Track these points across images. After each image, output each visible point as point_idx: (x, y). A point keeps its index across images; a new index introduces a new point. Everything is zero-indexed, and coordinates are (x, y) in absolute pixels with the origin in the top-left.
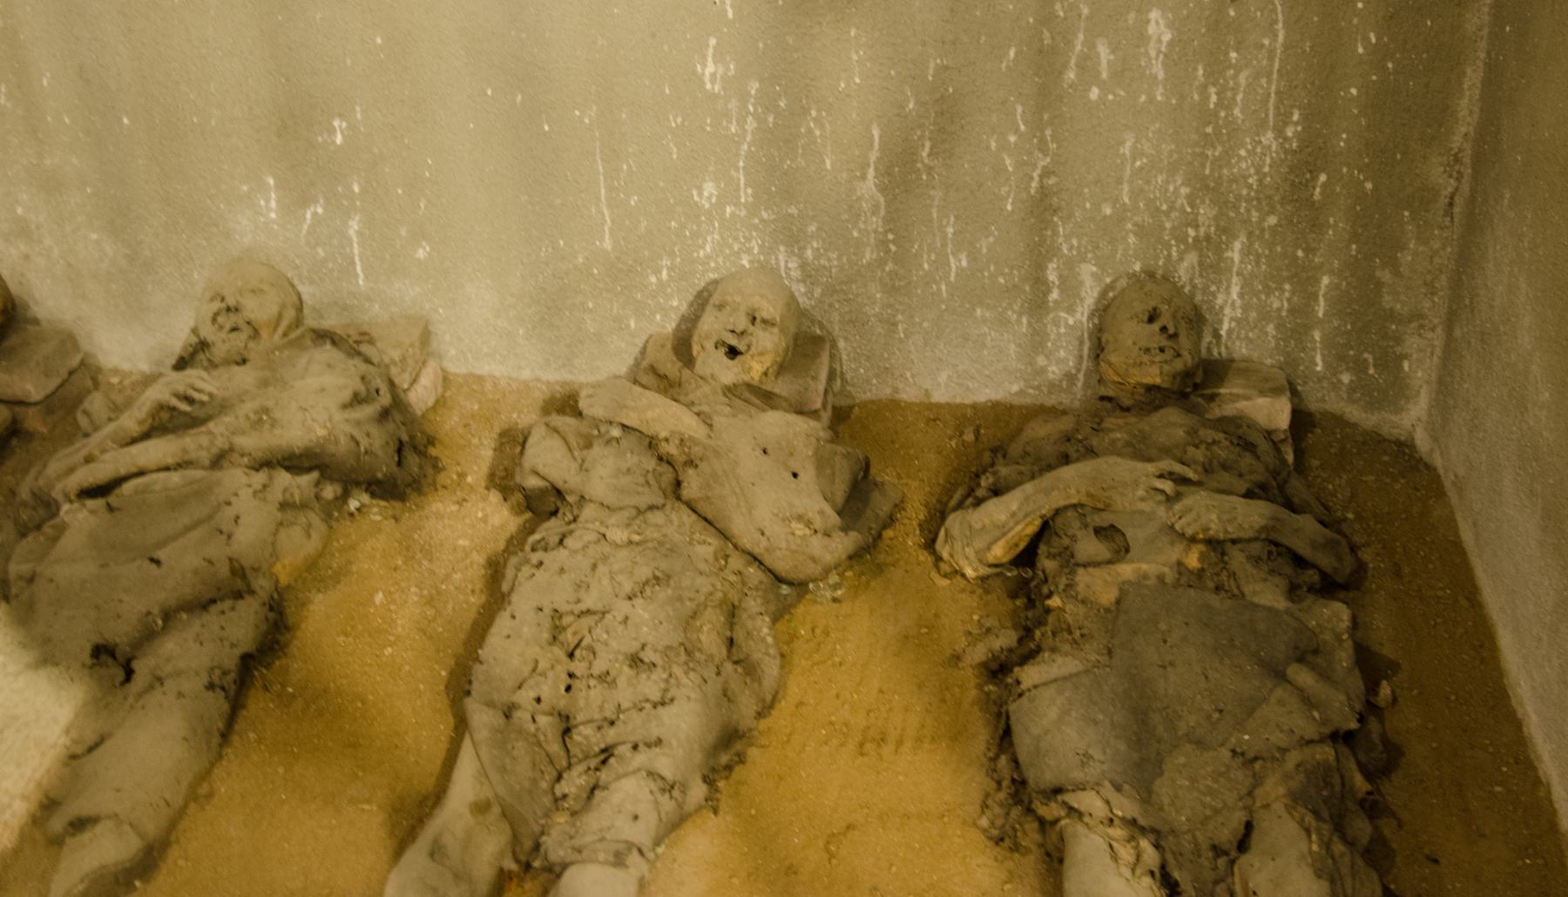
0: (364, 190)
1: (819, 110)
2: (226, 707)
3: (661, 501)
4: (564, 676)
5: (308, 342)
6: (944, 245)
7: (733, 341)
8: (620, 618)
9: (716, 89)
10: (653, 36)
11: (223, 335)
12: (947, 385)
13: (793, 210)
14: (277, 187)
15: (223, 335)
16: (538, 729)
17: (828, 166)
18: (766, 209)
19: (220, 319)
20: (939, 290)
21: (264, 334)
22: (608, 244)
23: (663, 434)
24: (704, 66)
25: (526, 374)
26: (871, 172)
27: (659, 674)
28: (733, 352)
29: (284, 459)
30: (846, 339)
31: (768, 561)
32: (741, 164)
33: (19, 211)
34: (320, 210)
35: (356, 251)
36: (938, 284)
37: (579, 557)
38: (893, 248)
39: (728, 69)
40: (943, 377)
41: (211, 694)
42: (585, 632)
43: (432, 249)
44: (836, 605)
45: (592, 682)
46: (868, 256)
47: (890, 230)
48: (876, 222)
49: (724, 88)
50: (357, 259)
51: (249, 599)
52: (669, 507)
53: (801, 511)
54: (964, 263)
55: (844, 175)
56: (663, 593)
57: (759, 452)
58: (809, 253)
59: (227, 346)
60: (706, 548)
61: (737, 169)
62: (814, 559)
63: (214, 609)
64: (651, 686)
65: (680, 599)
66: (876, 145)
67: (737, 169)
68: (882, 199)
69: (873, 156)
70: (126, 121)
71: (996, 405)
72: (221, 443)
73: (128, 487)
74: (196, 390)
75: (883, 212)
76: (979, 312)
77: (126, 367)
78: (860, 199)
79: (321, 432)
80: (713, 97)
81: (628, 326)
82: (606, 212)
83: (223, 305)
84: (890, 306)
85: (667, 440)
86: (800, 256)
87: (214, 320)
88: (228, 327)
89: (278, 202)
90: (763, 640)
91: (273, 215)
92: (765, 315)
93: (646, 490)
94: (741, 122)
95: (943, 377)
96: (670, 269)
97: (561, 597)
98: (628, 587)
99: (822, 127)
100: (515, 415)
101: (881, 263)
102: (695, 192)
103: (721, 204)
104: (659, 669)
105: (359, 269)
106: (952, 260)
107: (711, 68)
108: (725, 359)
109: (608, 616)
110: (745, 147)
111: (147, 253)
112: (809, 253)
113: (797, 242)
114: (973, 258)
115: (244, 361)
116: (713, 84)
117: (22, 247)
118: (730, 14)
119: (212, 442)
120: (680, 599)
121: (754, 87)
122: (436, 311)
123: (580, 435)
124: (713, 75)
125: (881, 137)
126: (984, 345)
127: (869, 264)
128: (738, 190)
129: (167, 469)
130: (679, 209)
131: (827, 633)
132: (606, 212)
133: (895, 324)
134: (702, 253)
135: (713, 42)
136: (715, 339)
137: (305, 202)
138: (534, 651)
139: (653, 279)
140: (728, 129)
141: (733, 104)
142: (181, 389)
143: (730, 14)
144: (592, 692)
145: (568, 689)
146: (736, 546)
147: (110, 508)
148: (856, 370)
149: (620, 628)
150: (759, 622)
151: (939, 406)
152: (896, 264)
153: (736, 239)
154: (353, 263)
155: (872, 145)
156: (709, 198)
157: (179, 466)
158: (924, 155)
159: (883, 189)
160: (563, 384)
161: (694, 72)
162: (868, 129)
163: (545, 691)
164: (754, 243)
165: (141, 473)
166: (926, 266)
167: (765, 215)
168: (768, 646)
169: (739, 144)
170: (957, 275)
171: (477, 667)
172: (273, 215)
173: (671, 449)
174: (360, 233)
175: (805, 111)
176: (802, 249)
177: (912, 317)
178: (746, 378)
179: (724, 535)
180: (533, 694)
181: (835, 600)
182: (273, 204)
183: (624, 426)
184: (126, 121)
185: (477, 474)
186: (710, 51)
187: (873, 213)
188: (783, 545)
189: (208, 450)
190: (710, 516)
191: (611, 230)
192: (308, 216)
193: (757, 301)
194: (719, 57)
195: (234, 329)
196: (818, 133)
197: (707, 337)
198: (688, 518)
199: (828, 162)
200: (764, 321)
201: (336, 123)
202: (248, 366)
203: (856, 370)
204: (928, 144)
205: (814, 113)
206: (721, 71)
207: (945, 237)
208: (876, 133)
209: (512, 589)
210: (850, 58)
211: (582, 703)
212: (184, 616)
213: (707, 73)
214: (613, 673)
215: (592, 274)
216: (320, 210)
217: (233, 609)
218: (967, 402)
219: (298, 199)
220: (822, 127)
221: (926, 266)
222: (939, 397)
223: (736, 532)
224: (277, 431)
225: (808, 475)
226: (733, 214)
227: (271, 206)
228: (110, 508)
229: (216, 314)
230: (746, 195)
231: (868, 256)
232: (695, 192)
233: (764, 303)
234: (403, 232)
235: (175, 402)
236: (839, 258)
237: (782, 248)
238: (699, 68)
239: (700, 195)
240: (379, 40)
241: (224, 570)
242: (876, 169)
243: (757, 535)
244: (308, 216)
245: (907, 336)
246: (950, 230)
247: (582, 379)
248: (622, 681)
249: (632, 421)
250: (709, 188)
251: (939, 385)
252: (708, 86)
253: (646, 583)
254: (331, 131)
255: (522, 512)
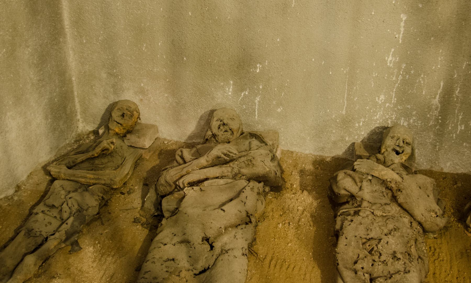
0: (263, 88)
1: (424, 75)
2: (146, 232)
3: (389, 202)
4: (371, 261)
5: (248, 137)
6: (458, 122)
7: (398, 149)
8: (386, 242)
9: (391, 65)
10: (373, 46)
11: (222, 133)
12: (449, 167)
13: (409, 107)
14: (233, 84)
15: (222, 133)
16: (365, 278)
17: (424, 93)
18: (400, 105)
19: (221, 127)
20: (453, 136)
21: (235, 133)
22: (344, 112)
23: (389, 180)
24: (388, 58)
25: (307, 152)
26: (438, 96)
27: (401, 262)
28: (398, 153)
29: (256, 178)
30: (418, 149)
31: (424, 225)
32: (395, 90)
33: (142, 85)
34: (247, 93)
35: (257, 107)
36: (453, 134)
37: (366, 219)
38: (440, 121)
39: (396, 59)
40: (448, 164)
41: (243, 257)
42: (374, 246)
43: (283, 109)
44: (436, 240)
45: (380, 263)
46: (431, 123)
47: (440, 116)
48: (436, 113)
49: (393, 65)
50: (256, 110)
51: (250, 224)
52: (391, 204)
53: (434, 209)
54: (463, 128)
55: (429, 97)
56: (397, 234)
57: (418, 188)
58: (412, 121)
59: (223, 137)
60: (406, 219)
61: (393, 92)
62: (437, 225)
63: (239, 227)
64: (399, 265)
65: (403, 236)
66: (441, 88)
67: (393, 92)
68: (440, 105)
69: (439, 92)
70: (185, 59)
71: (465, 174)
72: (236, 170)
73: (206, 183)
74: (231, 153)
75: (439, 110)
76: (465, 144)
77: (168, 138)
78: (432, 105)
79: (268, 169)
80: (389, 68)
81: (346, 139)
82: (345, 102)
83: (222, 123)
84: (435, 140)
85: (390, 182)
86: (408, 121)
87: (219, 128)
88: (224, 130)
89: (232, 89)
90: (423, 251)
91: (230, 93)
92: (407, 141)
93: (384, 198)
94: (397, 77)
95: (448, 164)
96: (364, 122)
97: (361, 232)
98: (386, 231)
99: (424, 80)
100: (303, 165)
101: (435, 126)
102: (377, 98)
103: (385, 102)
104: (401, 260)
105: (256, 113)
106: (459, 127)
107: (390, 58)
108: (396, 155)
109: (382, 241)
110: (397, 85)
111: (184, 102)
112: (412, 121)
113: (408, 117)
114: (466, 127)
115: (229, 142)
116: (390, 63)
117: (141, 97)
118: (400, 42)
119: (232, 170)
120: (403, 236)
121: (404, 66)
122: (280, 129)
123: (359, 178)
124: (391, 61)
125: (443, 85)
126: (464, 155)
127: (431, 126)
128: (392, 98)
129: (217, 178)
130: (370, 103)
131: (435, 250)
132: (345, 102)
133: (436, 146)
134: (375, 118)
135: (393, 50)
136: (392, 148)
137: (242, 90)
138: (357, 251)
139: (357, 125)
140: (392, 79)
141: (396, 71)
142: (225, 152)
143: (400, 42)
144: (380, 267)
145: (372, 265)
146: (415, 220)
147: (201, 190)
148: (420, 159)
149: (386, 245)
150: (422, 245)
151: (446, 174)
152: (440, 126)
153: (388, 114)
154: (255, 111)
155: (440, 88)
156: (382, 100)
157: (222, 177)
158: (457, 92)
159: (441, 102)
160: (320, 156)
161: (385, 59)
162: (440, 83)
163: (365, 265)
164: (393, 116)
165: (207, 179)
166: (450, 128)
167: (399, 107)
168: (424, 254)
169: (395, 84)
170: (460, 132)
171: (337, 255)
172: (230, 93)
173: (393, 185)
174: (259, 102)
175: (420, 75)
176: (409, 119)
177: (442, 144)
178: (401, 161)
179: (411, 215)
180: (361, 266)
181: (435, 238)
182: (231, 90)
183: (373, 176)
184: (185, 59)
185: (296, 185)
186: (391, 53)
187: (436, 110)
188: (429, 220)
189: (231, 172)
190: (407, 209)
191: (346, 108)
192: (242, 95)
193: (405, 137)
194: (393, 55)
195: (226, 131)
196: (422, 82)
197: (389, 147)
198: (398, 209)
199: (424, 92)
200: (407, 143)
201: (258, 66)
202: (231, 143)
203: (420, 159)
204: (459, 89)
205: (422, 76)
206: (394, 60)
207: (458, 120)
208: (442, 84)
209: (342, 228)
210: (438, 59)
211: (376, 270)
212: (230, 229)
213: (389, 60)
214: (387, 261)
215: (336, 122)
216: (247, 93)
217: (245, 228)
218: (455, 173)
219: (240, 89)
220: (424, 80)
221: (450, 128)
222: (445, 170)
223: (416, 214)
224: (254, 168)
225: (431, 196)
226: (388, 106)
227: (230, 90)
228: (201, 190)
229: (220, 125)
230: (394, 100)
231: (431, 123)
232: (377, 98)
233: (407, 137)
234: (274, 103)
235: (223, 156)
236: (421, 123)
237: (403, 118)
238: (386, 58)
239: (379, 99)
240: (278, 40)
241: (244, 214)
242: (440, 95)
243: (422, 216)
244: (242, 95)
245: (439, 150)
246: (461, 117)
247: (326, 155)
248: (389, 264)
249: (376, 174)
250: (382, 97)
251: (446, 166)
252: (388, 64)
253: (392, 230)
254: (256, 68)
255: (317, 199)
